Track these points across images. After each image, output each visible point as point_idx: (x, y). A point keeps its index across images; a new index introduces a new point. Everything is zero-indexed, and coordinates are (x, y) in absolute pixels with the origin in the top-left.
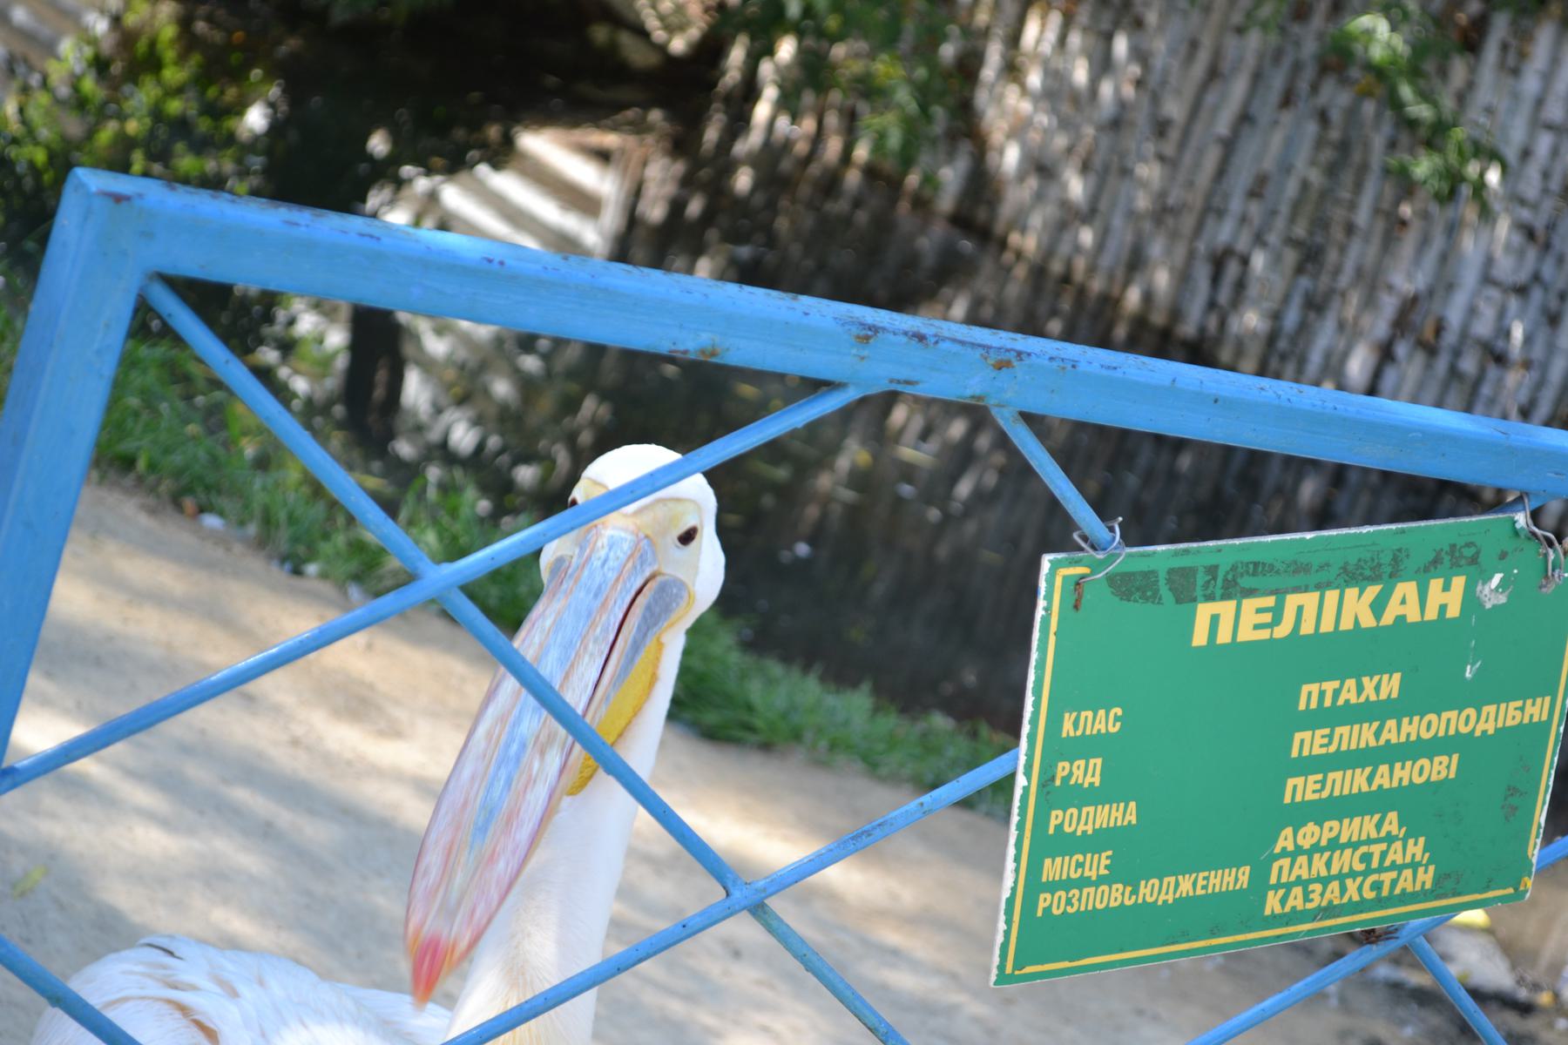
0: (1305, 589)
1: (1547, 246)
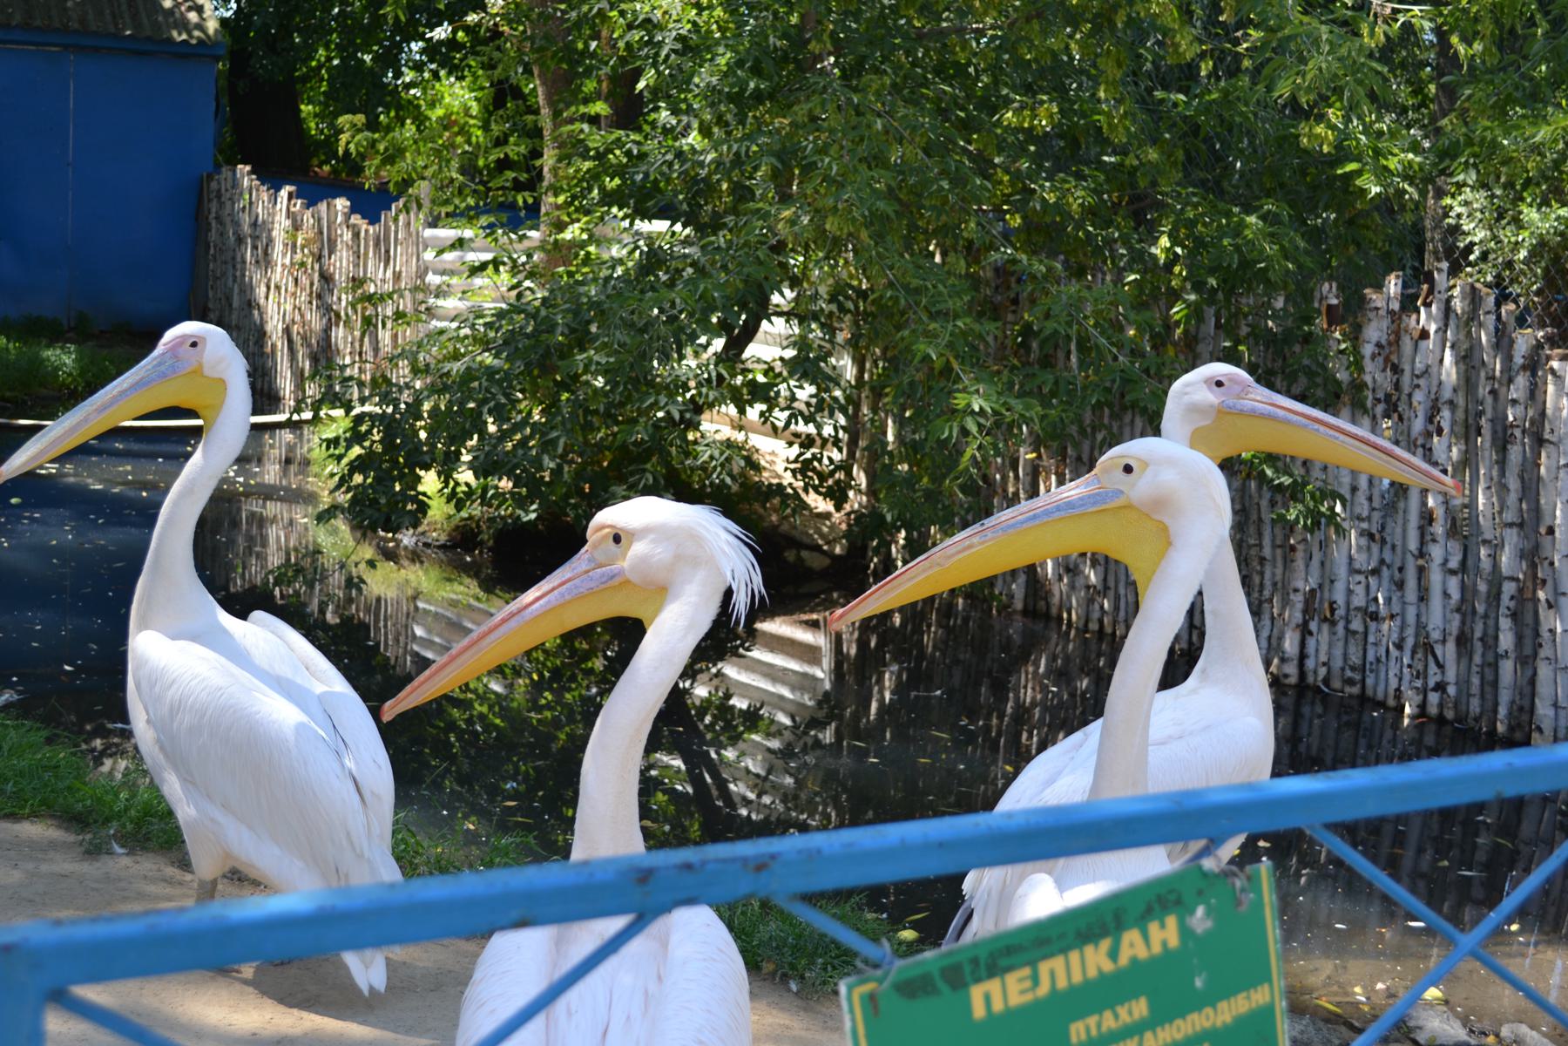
0: (1052, 955)
1: (1383, 541)
